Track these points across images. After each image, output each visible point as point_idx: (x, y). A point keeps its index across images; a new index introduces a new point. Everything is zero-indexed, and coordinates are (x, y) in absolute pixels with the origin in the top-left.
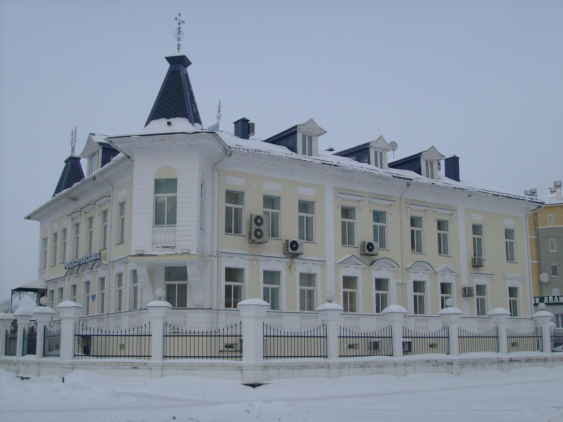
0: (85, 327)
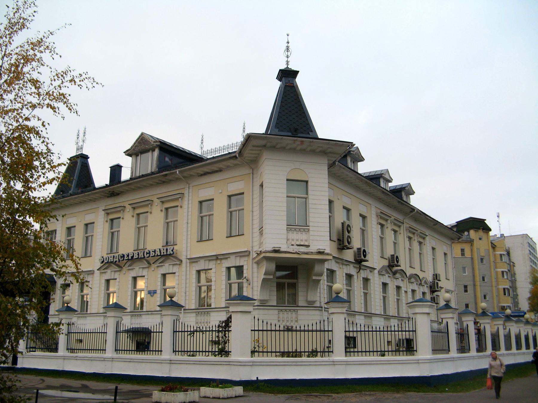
0: (351, 322)
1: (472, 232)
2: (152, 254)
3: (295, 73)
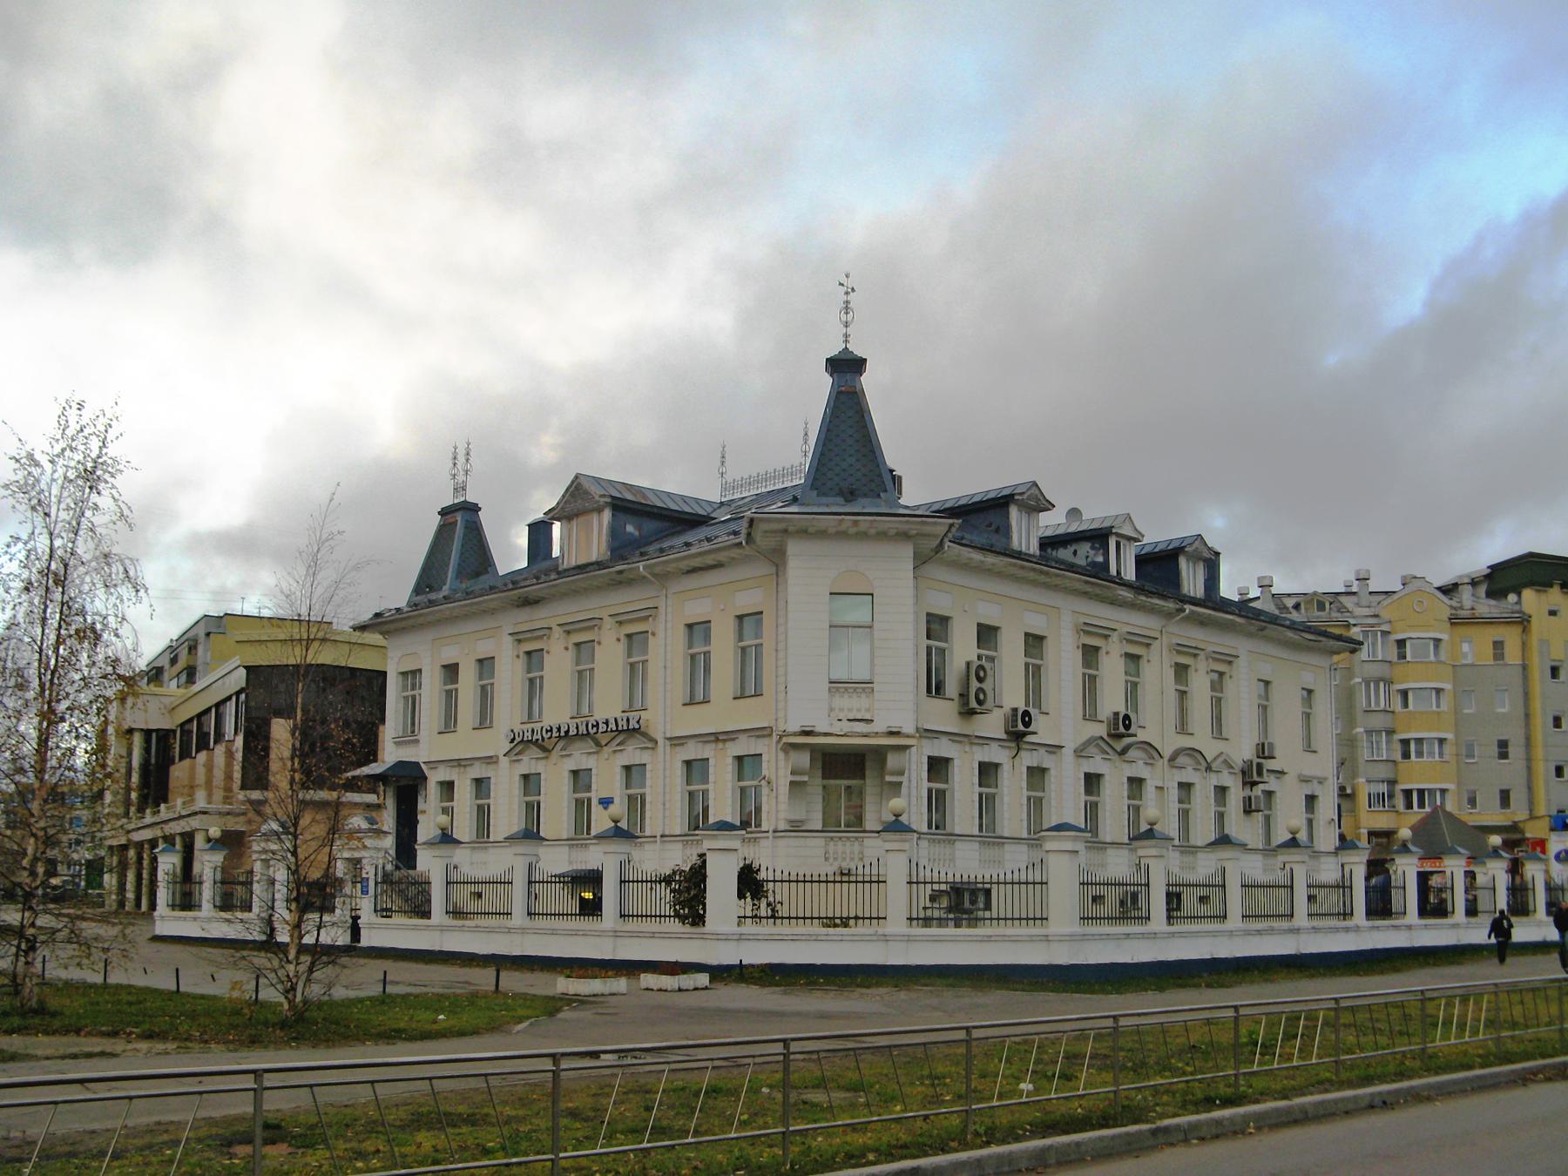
1: (1528, 594)
2: (602, 727)
3: (858, 365)
